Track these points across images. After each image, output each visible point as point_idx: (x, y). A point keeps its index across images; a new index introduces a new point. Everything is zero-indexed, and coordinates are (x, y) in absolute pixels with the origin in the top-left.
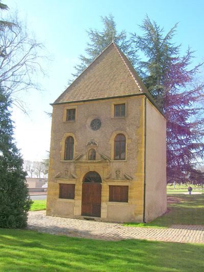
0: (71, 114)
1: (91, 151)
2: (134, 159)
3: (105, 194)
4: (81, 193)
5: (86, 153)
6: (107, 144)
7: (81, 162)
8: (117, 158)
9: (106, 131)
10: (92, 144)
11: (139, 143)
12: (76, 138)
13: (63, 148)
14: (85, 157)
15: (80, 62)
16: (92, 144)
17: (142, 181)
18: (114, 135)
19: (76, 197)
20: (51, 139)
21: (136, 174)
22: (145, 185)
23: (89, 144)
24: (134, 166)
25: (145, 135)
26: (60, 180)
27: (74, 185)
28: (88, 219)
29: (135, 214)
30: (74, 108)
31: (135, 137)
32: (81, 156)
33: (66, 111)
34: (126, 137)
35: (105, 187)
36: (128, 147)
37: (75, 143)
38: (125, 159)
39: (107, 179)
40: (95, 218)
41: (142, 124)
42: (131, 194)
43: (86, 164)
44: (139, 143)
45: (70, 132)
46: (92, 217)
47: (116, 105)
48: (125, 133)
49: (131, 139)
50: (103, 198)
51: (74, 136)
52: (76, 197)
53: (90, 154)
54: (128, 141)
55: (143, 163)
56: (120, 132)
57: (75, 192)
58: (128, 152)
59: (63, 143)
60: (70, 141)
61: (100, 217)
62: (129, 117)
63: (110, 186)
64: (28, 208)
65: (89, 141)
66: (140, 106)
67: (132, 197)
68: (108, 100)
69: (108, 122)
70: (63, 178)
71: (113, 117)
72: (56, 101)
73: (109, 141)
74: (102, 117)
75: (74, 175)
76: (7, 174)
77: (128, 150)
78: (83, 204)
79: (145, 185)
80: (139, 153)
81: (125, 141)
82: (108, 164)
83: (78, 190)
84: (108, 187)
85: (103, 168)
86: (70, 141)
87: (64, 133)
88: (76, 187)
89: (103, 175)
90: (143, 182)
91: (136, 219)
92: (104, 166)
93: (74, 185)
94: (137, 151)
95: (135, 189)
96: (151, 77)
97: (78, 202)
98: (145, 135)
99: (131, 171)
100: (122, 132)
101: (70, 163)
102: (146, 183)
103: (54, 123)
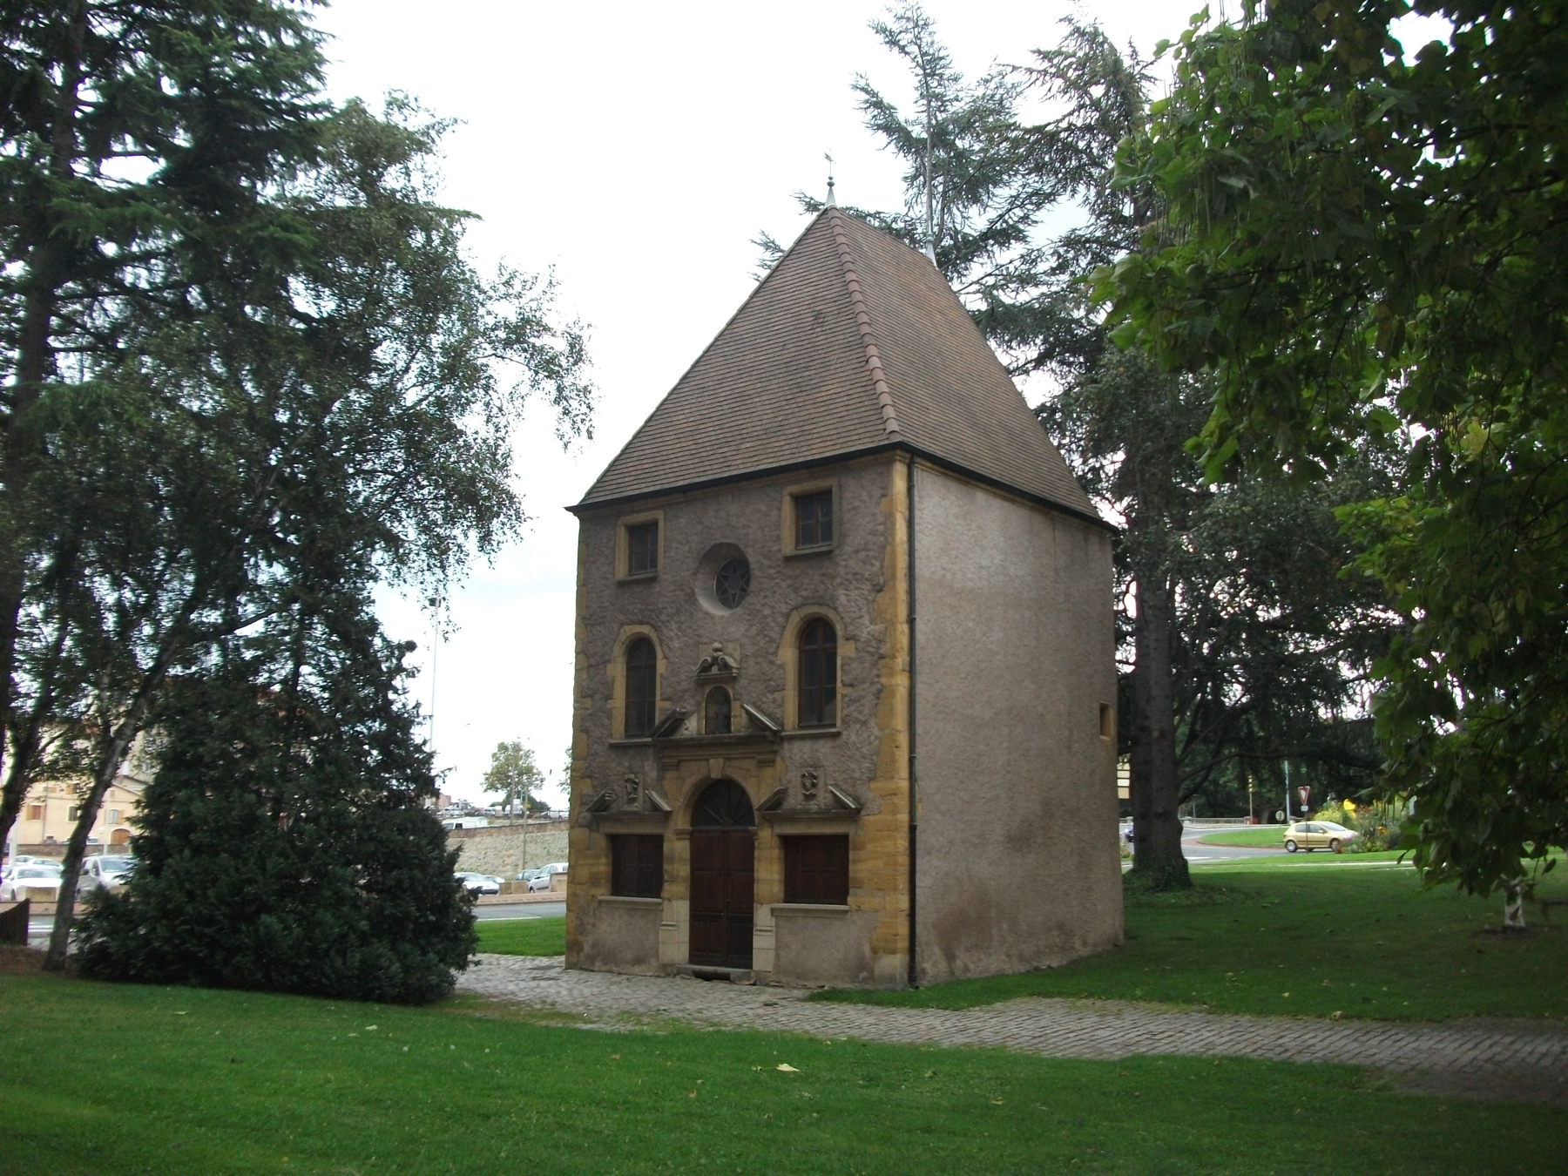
0: (643, 535)
3: (769, 873)
6: (772, 663)
8: (804, 724)
11: (882, 657)
13: (620, 690)
17: (895, 812)
19: (668, 889)
20: (577, 653)
21: (873, 785)
22: (912, 829)
24: (865, 750)
25: (911, 621)
28: (707, 977)
31: (867, 629)
33: (623, 529)
35: (767, 845)
36: (843, 671)
37: (661, 667)
41: (894, 576)
42: (862, 866)
44: (882, 657)
48: (832, 615)
50: (760, 890)
52: (666, 886)
54: (845, 650)
55: (903, 740)
59: (617, 670)
60: (640, 653)
61: (750, 967)
62: (847, 549)
64: (99, 807)
66: (883, 496)
71: (788, 546)
72: (589, 494)
73: (775, 653)
76: (1495, 770)
77: (844, 685)
78: (696, 917)
79: (912, 829)
80: (883, 695)
86: (640, 653)
89: (758, 794)
90: (904, 817)
96: (1182, 206)
97: (677, 911)
98: (911, 621)
99: (857, 775)
102: (920, 824)
103: (584, 585)
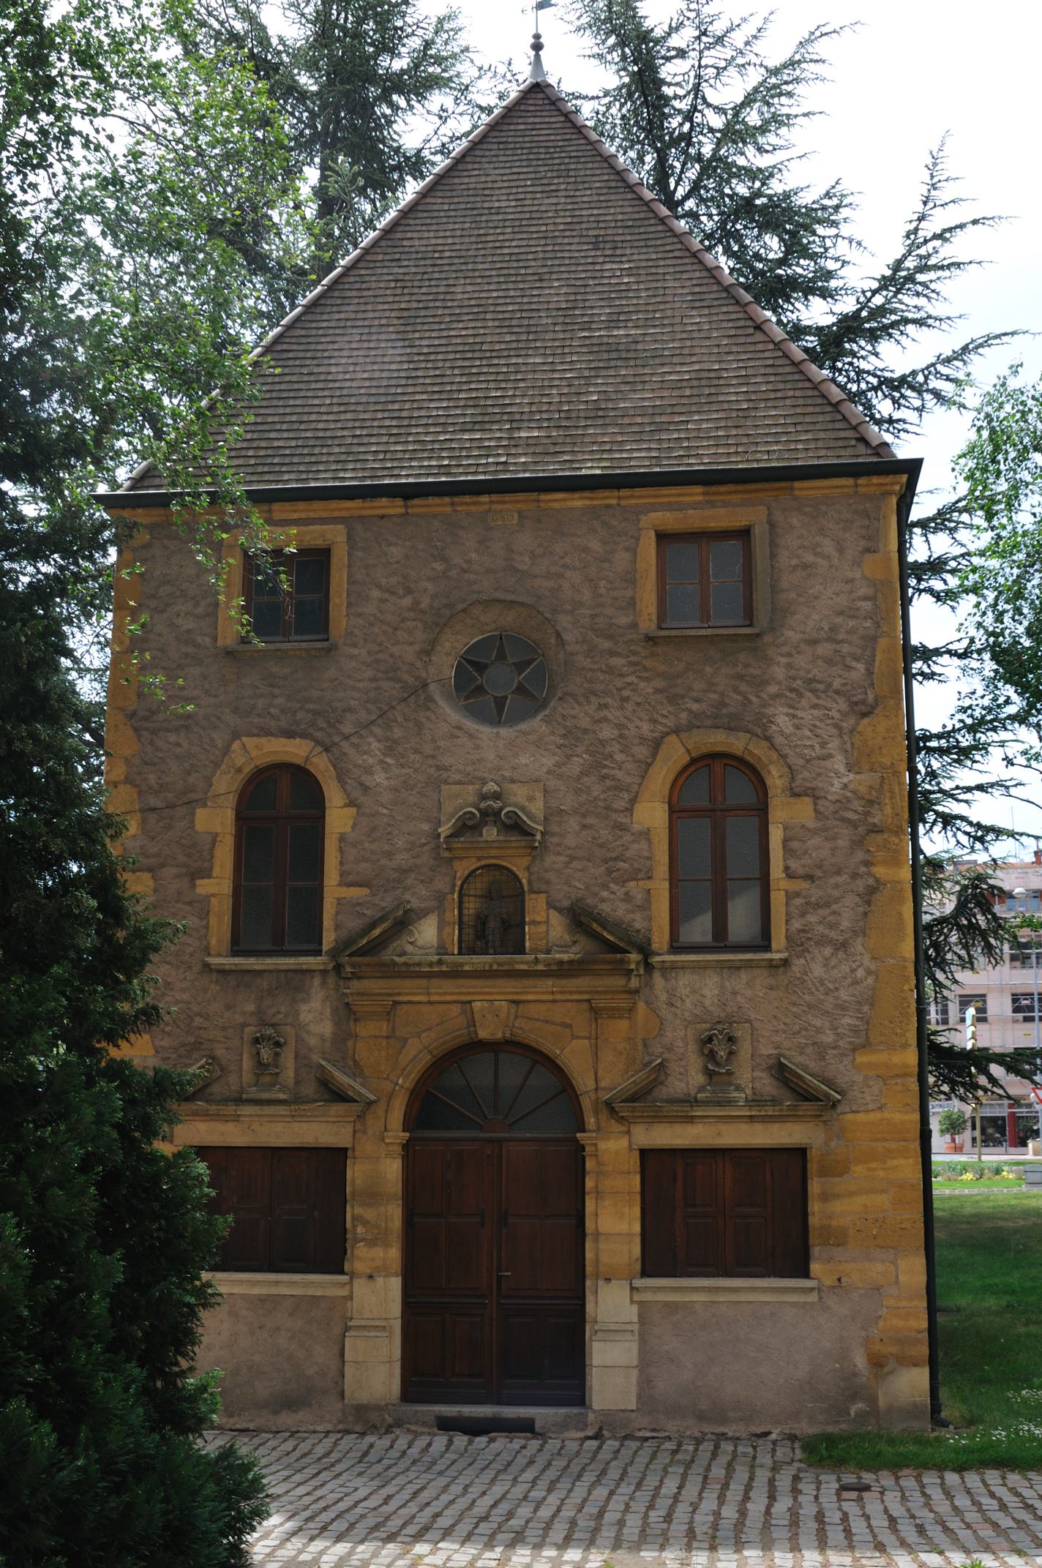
1: (478, 886)
2: (843, 946)
4: (395, 1213)
5: (440, 898)
6: (622, 828)
7: (410, 972)
9: (607, 732)
10: (490, 833)
11: (876, 830)
12: (341, 777)
14: (427, 932)
15: (463, 40)
16: (490, 833)
18: (675, 755)
19: (362, 1256)
21: (862, 1058)
23: (467, 827)
24: (844, 995)
26: (206, 1116)
27: (336, 1158)
28: (474, 1428)
29: (877, 1363)
30: (319, 543)
32: (403, 922)
34: (776, 779)
37: (338, 819)
38: (767, 947)
39: (632, 1099)
40: (540, 1414)
43: (449, 985)
44: (876, 830)
45: (289, 734)
46: (510, 1412)
47: (214, 842)
48: (759, 750)
49: (813, 794)
51: (321, 766)
53: (472, 906)
56: (718, 740)
57: (637, 1228)
58: (790, 896)
63: (643, 1153)
65: (460, 800)
67: (837, 1238)
68: (608, 498)
69: (617, 662)
70: (239, 1101)
73: (629, 810)
74: (564, 621)
75: (342, 1078)
77: (790, 875)
81: (761, 810)
82: (634, 983)
83: (372, 1196)
84: (635, 1159)
85: (595, 1012)
87: (236, 735)
88: (356, 1174)
91: (882, 1402)
92: (600, 1002)
93: (336, 1158)
94: (860, 885)
95: (859, 1170)
99: (828, 1038)
100: (737, 743)
101: (294, 983)
